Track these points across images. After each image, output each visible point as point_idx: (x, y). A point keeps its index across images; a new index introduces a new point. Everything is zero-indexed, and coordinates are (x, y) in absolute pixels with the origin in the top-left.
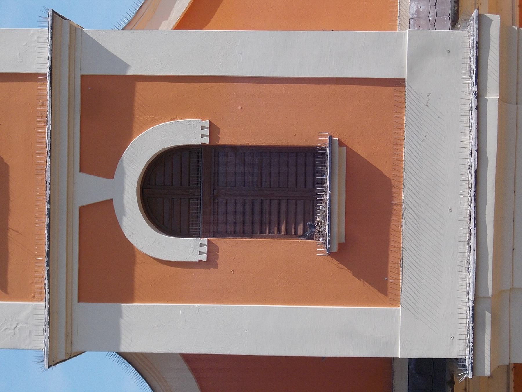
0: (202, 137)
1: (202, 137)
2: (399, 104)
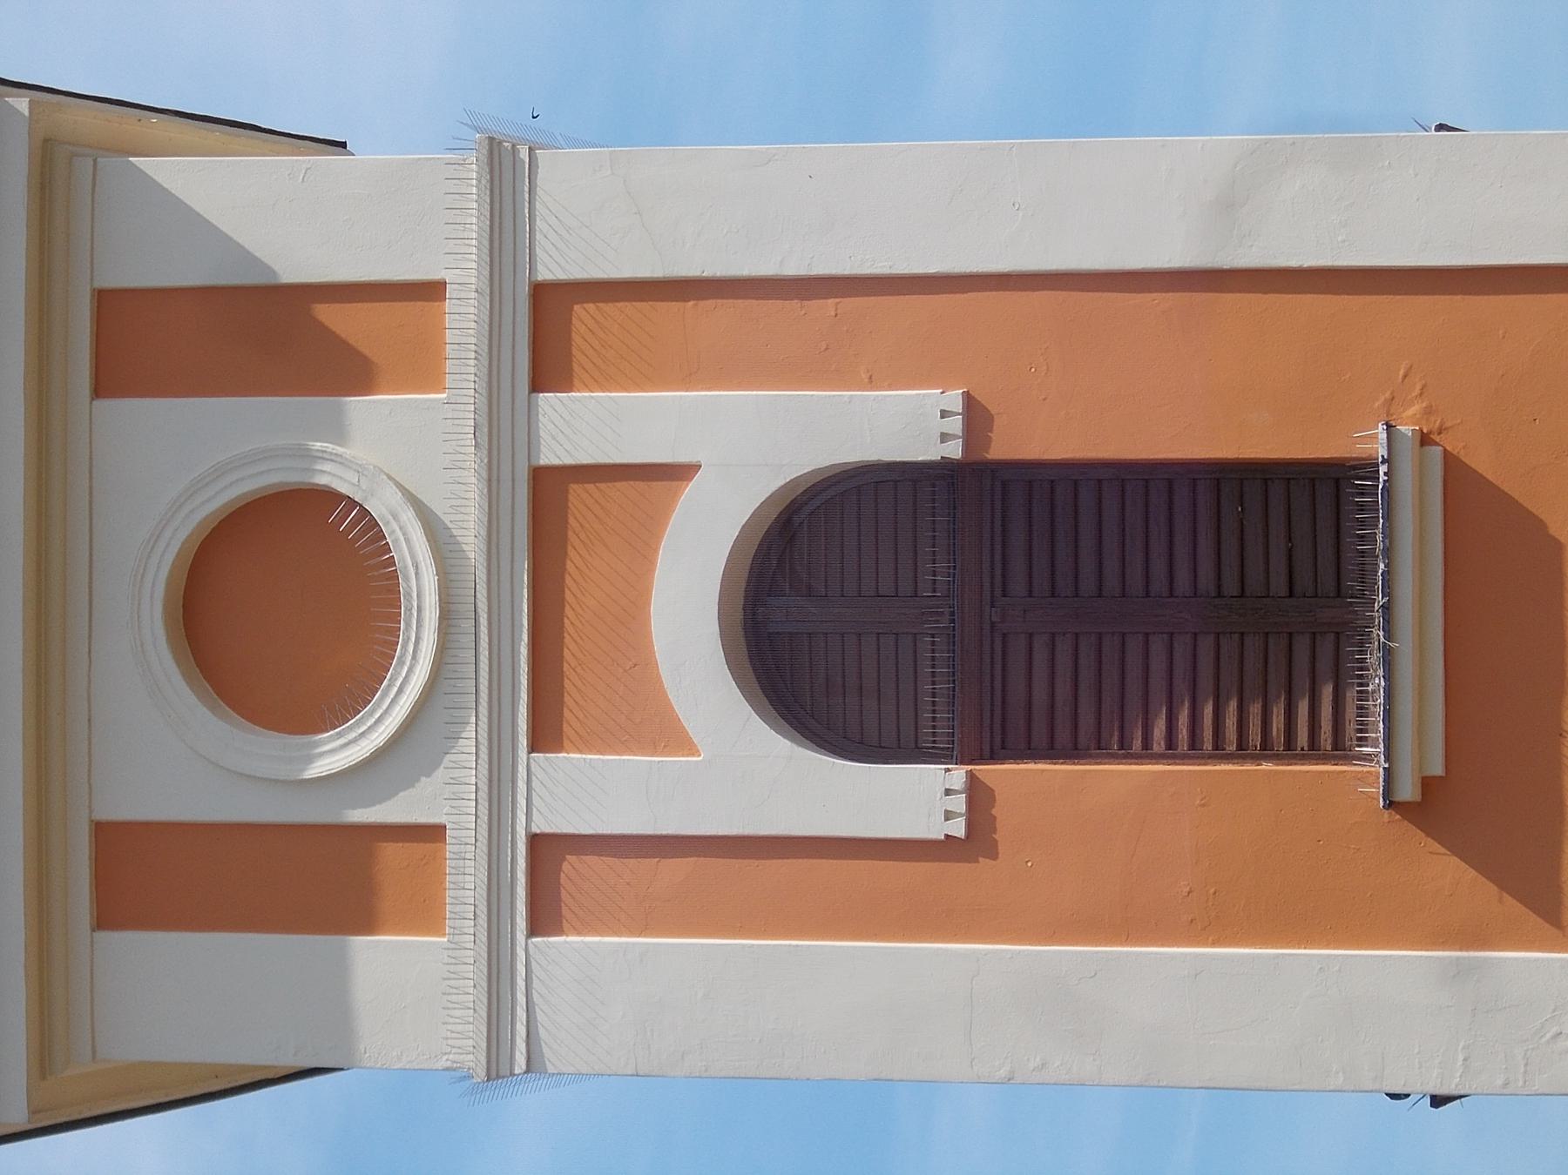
0: (947, 819)
1: (947, 819)
2: (438, 861)
